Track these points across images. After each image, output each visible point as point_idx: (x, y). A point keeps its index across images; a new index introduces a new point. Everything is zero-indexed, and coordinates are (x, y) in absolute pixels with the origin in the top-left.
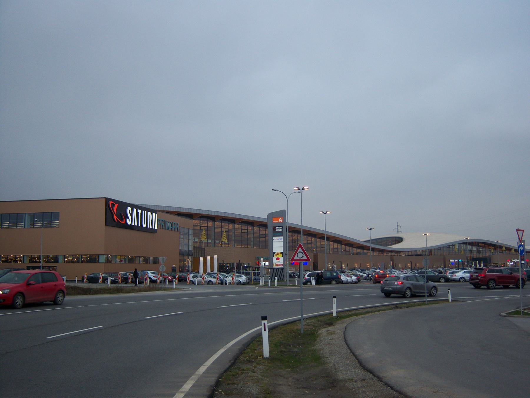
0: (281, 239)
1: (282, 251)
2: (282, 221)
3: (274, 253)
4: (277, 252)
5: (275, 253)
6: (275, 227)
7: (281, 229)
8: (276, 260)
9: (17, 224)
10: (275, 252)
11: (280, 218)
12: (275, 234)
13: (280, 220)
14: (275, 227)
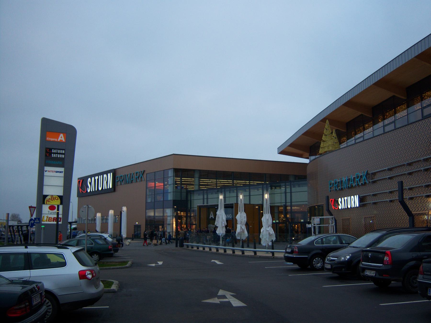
0: (60, 172)
1: (61, 194)
2: (64, 140)
3: (46, 196)
4: (52, 196)
5: (48, 197)
6: (51, 149)
7: (62, 154)
8: (49, 210)
9: (186, 188)
10: (47, 196)
11: (62, 135)
12: (49, 162)
13: (62, 138)
14: (51, 149)
